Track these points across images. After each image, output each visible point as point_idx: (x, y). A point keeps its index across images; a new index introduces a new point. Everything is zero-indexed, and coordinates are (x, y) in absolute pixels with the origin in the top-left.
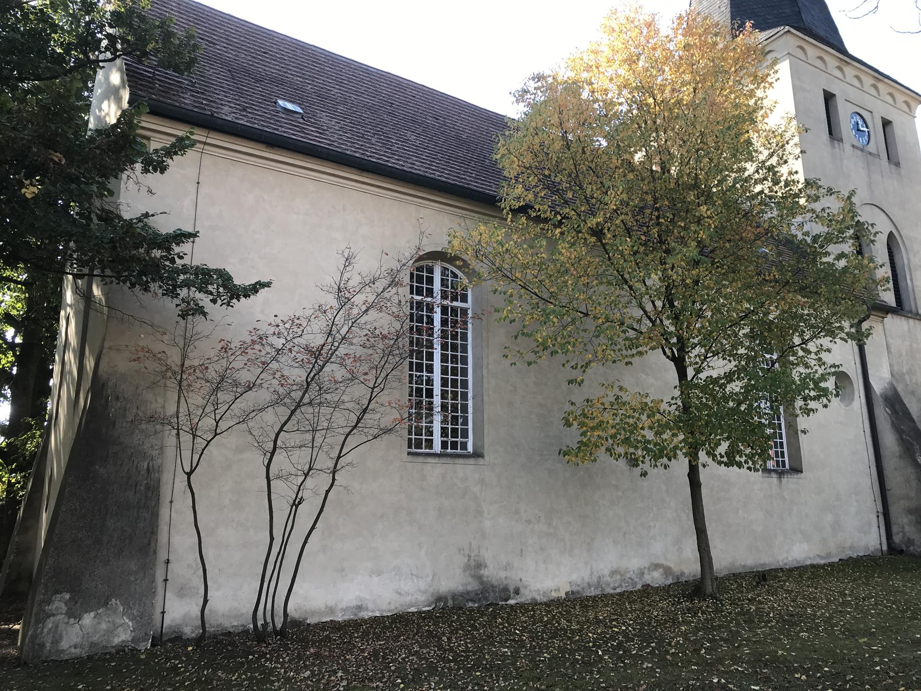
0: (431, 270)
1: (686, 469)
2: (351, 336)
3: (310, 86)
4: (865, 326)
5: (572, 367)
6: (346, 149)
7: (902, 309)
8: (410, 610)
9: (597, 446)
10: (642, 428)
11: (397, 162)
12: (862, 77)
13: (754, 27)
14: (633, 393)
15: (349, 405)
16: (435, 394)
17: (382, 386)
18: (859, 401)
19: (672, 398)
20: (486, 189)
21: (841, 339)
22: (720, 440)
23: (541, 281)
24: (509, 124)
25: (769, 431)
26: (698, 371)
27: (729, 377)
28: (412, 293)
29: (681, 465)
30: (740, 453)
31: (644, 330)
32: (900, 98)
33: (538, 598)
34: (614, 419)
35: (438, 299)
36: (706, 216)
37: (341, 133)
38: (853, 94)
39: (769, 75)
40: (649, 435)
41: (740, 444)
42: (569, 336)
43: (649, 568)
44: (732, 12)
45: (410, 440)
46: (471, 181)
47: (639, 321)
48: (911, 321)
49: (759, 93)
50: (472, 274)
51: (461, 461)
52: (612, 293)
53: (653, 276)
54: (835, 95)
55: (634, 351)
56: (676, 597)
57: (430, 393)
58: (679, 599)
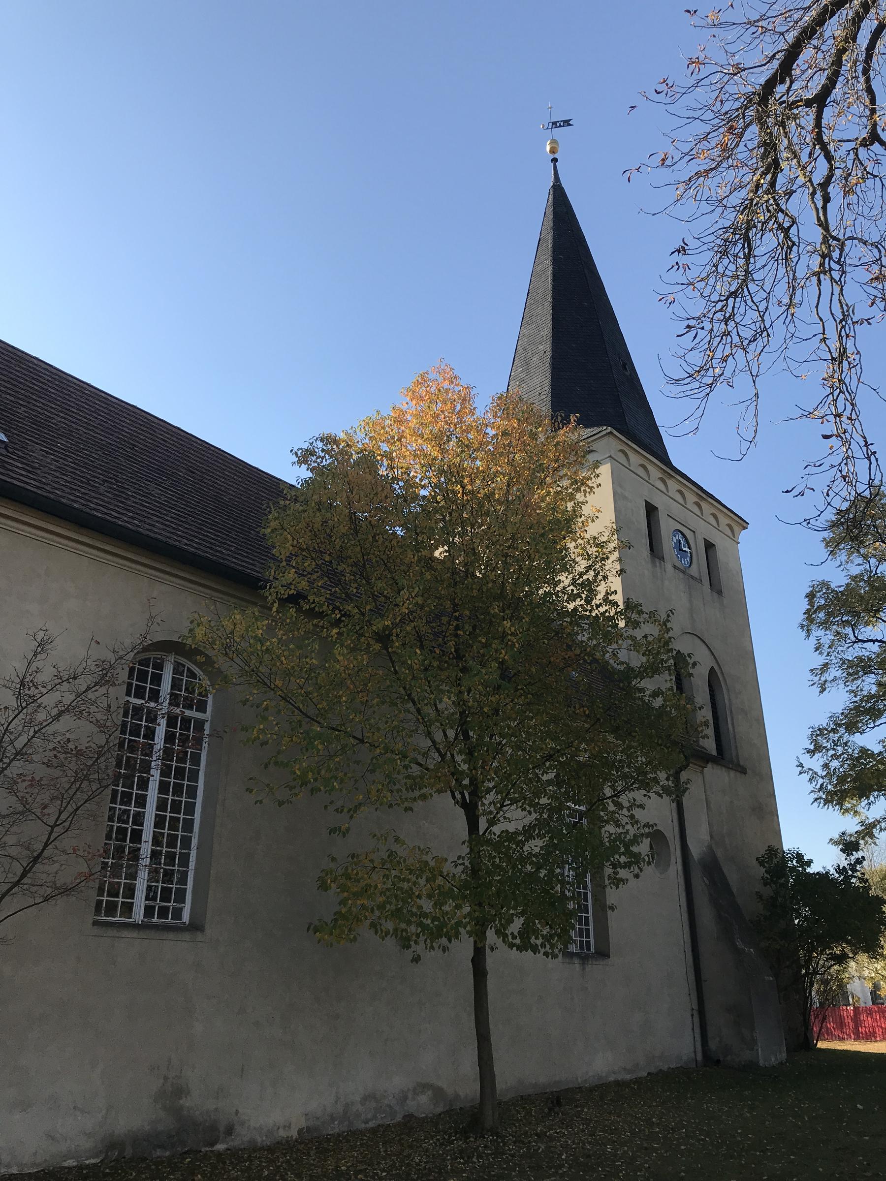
0: (159, 666)
1: (471, 953)
2: (30, 751)
3: (23, 409)
4: (684, 776)
5: (337, 810)
6: (61, 496)
7: (723, 759)
8: (66, 1164)
9: (358, 920)
10: (419, 897)
11: (131, 520)
12: (687, 493)
13: (579, 422)
14: (411, 846)
15: (14, 851)
16: (143, 839)
17: (67, 824)
18: (676, 867)
19: (459, 857)
20: (248, 568)
21: (656, 793)
22: (513, 914)
23: (307, 694)
24: (285, 492)
25: (571, 905)
26: (492, 823)
27: (528, 832)
28: (128, 694)
29: (464, 948)
30: (536, 933)
31: (431, 767)
32: (724, 521)
33: (259, 1140)
34: (384, 883)
35: (164, 706)
36: (510, 633)
37: (58, 474)
38: (676, 509)
39: (589, 479)
40: (427, 906)
41: (537, 921)
42: (337, 769)
43: (415, 1089)
44: (552, 402)
45: (99, 903)
46: (228, 555)
47: (425, 755)
48: (732, 773)
49: (579, 497)
50: (215, 674)
51: (171, 936)
52: (395, 716)
53: (445, 699)
55: (417, 793)
56: (445, 1133)
57: (137, 836)
58: (450, 1137)
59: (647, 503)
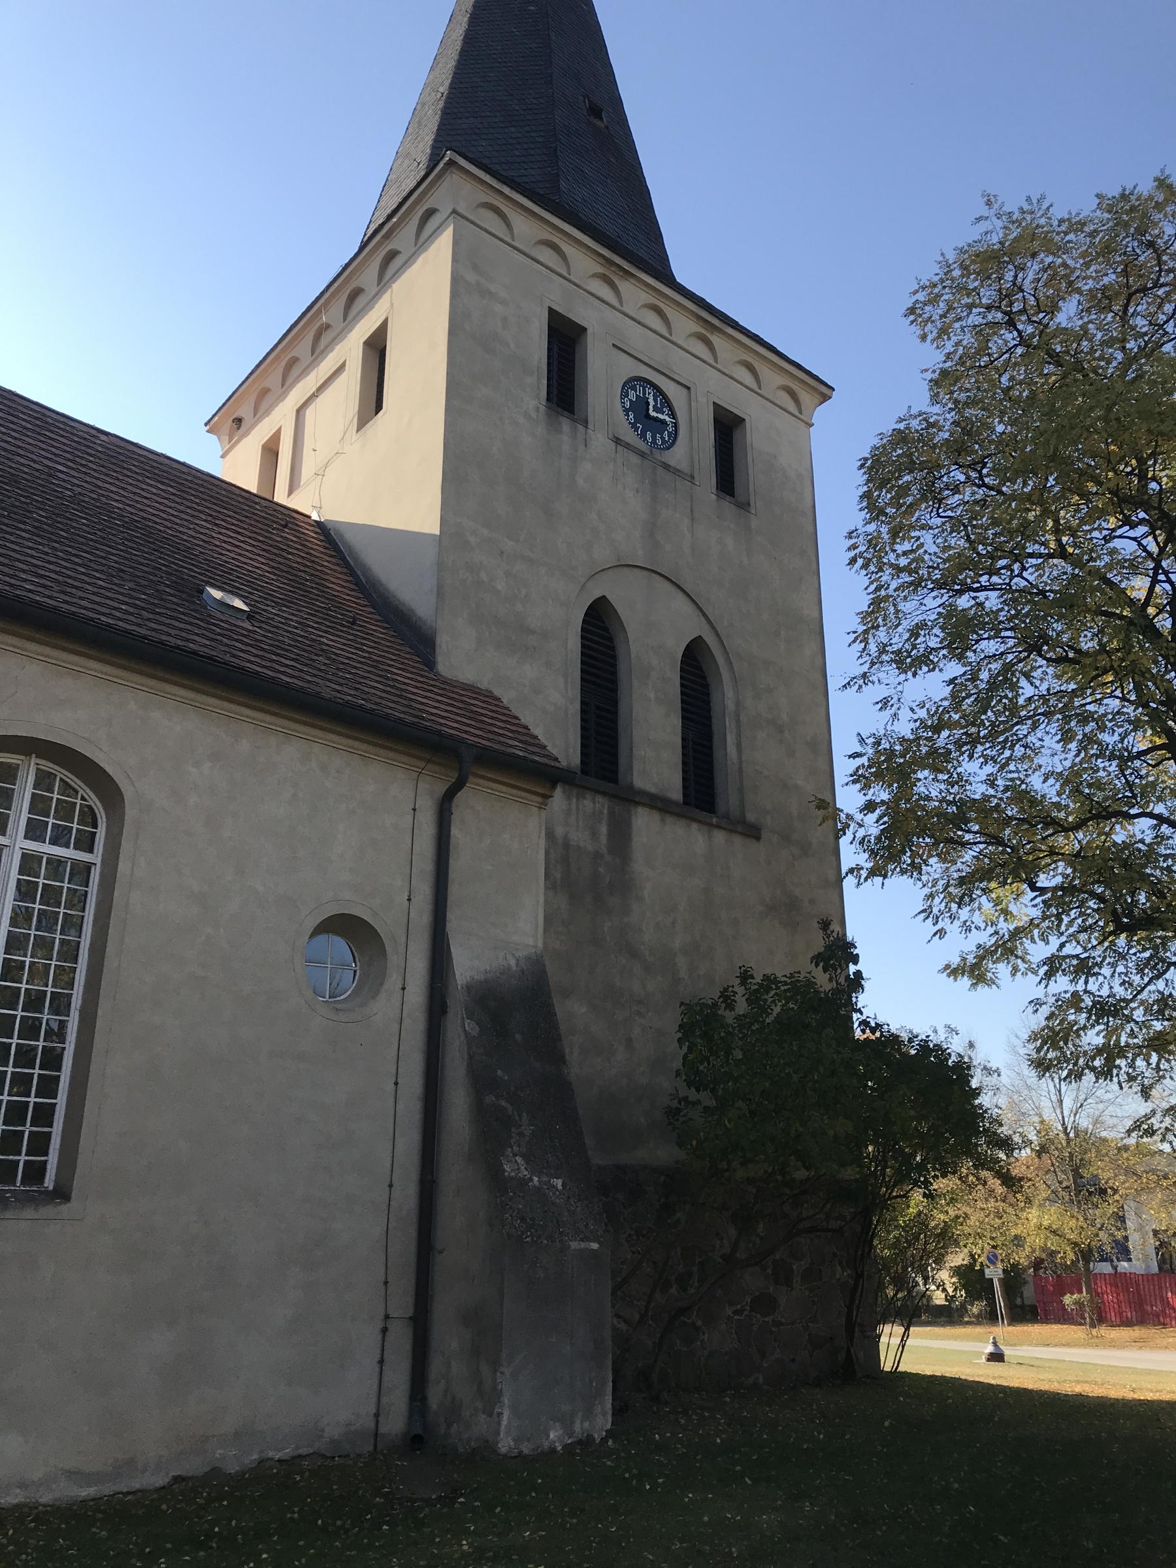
12: (669, 311)
38: (636, 337)
54: (584, 330)
59: (556, 320)
